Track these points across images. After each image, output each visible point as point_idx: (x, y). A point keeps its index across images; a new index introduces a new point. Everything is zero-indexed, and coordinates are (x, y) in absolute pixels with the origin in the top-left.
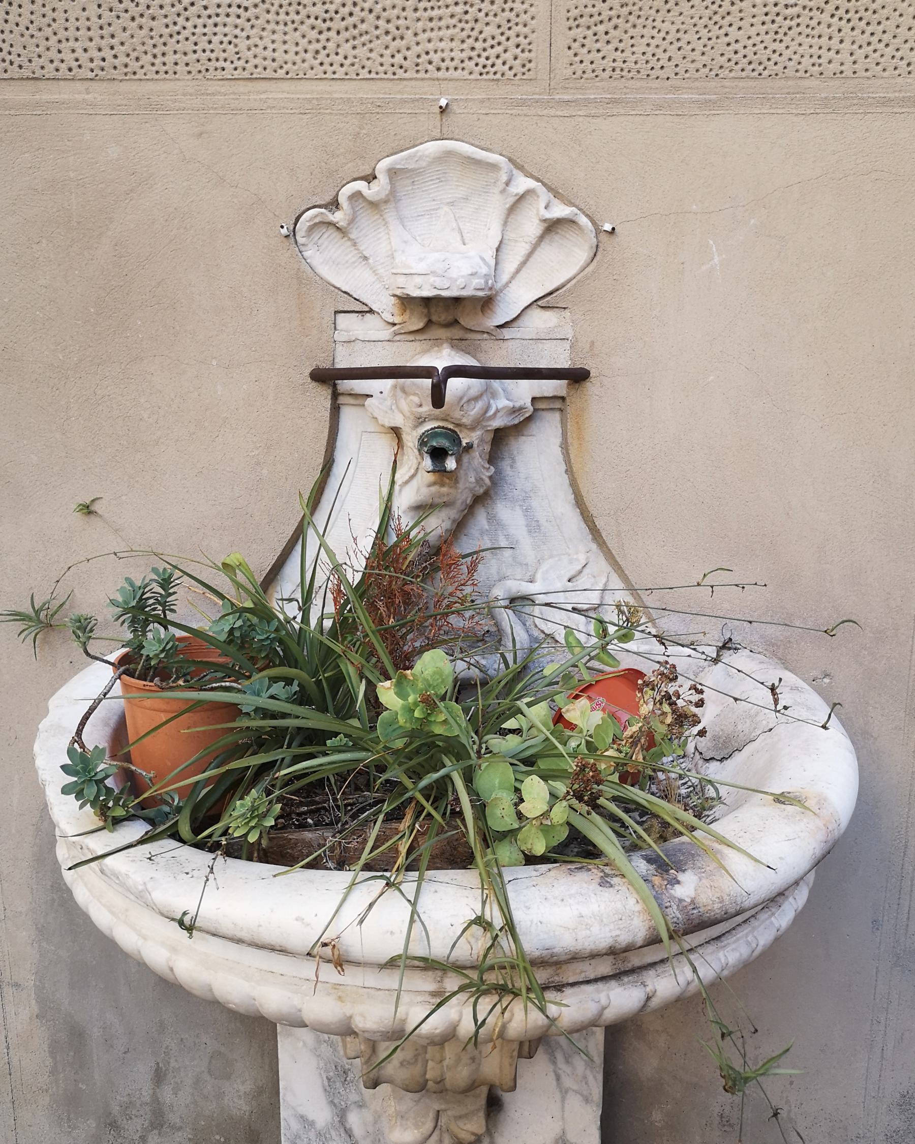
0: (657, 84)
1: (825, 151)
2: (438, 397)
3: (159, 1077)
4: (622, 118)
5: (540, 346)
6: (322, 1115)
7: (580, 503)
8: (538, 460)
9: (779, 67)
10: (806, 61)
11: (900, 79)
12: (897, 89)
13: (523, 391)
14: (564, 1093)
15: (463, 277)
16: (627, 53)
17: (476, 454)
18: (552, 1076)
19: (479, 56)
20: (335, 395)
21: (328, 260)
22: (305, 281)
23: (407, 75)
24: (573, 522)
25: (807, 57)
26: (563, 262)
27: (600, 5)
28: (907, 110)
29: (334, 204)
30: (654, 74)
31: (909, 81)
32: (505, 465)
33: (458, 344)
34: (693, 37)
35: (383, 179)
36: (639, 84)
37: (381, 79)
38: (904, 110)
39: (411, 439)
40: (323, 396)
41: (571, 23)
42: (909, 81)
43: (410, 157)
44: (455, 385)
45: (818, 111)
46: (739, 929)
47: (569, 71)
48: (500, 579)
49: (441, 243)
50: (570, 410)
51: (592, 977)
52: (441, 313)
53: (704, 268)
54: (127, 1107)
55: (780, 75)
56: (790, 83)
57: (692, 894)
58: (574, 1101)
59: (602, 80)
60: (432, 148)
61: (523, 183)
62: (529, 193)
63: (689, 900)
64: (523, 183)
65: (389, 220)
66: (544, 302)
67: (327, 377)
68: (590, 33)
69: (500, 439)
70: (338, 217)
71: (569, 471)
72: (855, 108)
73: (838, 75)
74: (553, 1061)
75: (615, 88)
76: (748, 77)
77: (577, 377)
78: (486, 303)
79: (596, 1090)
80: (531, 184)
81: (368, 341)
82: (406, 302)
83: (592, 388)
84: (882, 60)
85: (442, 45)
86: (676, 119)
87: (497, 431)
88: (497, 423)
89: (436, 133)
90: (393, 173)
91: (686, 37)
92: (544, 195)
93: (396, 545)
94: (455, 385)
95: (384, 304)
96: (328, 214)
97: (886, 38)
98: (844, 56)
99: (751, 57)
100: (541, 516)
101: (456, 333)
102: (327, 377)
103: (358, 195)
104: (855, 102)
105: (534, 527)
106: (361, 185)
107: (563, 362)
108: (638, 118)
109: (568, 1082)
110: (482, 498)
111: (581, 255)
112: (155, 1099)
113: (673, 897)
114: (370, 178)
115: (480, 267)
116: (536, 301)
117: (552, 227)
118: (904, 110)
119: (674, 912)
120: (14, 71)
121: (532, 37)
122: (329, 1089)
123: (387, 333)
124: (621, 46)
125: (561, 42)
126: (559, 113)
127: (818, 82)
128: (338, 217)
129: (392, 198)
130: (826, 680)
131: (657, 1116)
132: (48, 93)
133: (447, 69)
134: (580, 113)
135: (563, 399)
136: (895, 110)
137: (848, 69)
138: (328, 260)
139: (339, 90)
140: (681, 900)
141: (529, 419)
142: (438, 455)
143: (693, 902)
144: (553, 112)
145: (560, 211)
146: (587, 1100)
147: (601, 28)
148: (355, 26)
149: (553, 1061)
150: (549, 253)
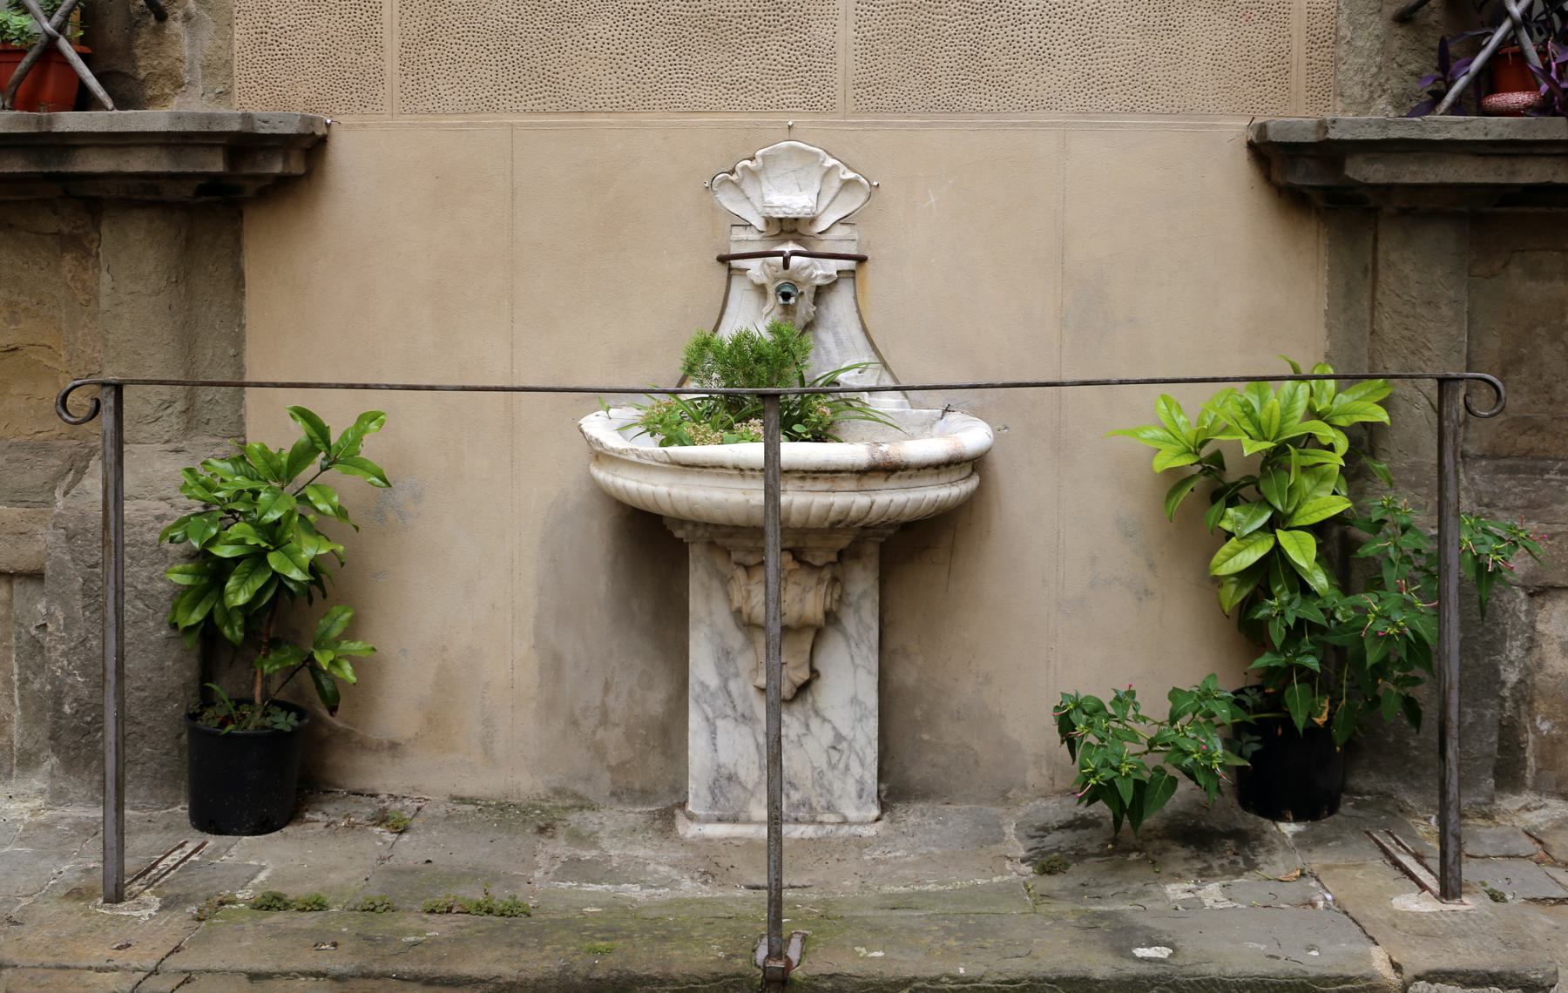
2: (786, 265)
3: (607, 688)
6: (713, 682)
7: (865, 330)
8: (841, 305)
13: (833, 266)
14: (856, 667)
17: (806, 297)
18: (848, 658)
20: (730, 269)
21: (729, 201)
22: (716, 209)
24: (861, 340)
26: (850, 203)
29: (733, 172)
32: (822, 308)
33: (797, 241)
35: (760, 160)
39: (771, 290)
40: (722, 271)
44: (795, 260)
48: (817, 369)
49: (790, 197)
50: (858, 276)
52: (789, 228)
54: (585, 709)
58: (862, 674)
60: (784, 144)
61: (830, 162)
62: (834, 167)
64: (830, 162)
66: (841, 221)
67: (724, 259)
69: (820, 293)
70: (734, 178)
71: (858, 311)
74: (849, 646)
77: (861, 260)
78: (812, 221)
79: (875, 668)
80: (835, 162)
81: (747, 240)
82: (768, 221)
83: (868, 265)
87: (818, 287)
88: (819, 282)
90: (764, 157)
92: (843, 168)
93: (619, 867)
94: (795, 260)
95: (759, 223)
96: (732, 177)
100: (843, 336)
101: (796, 236)
102: (724, 259)
103: (746, 167)
105: (839, 343)
106: (747, 163)
107: (853, 252)
109: (858, 661)
110: (809, 326)
111: (863, 198)
112: (603, 703)
114: (752, 159)
115: (574, 868)
117: (847, 184)
120: (572, 108)
122: (718, 666)
123: (757, 237)
125: (850, 95)
128: (734, 178)
129: (764, 169)
131: (918, 713)
132: (587, 119)
138: (729, 201)
139: (738, 118)
141: (836, 282)
142: (786, 296)
145: (850, 175)
146: (869, 673)
149: (849, 646)
150: (843, 197)
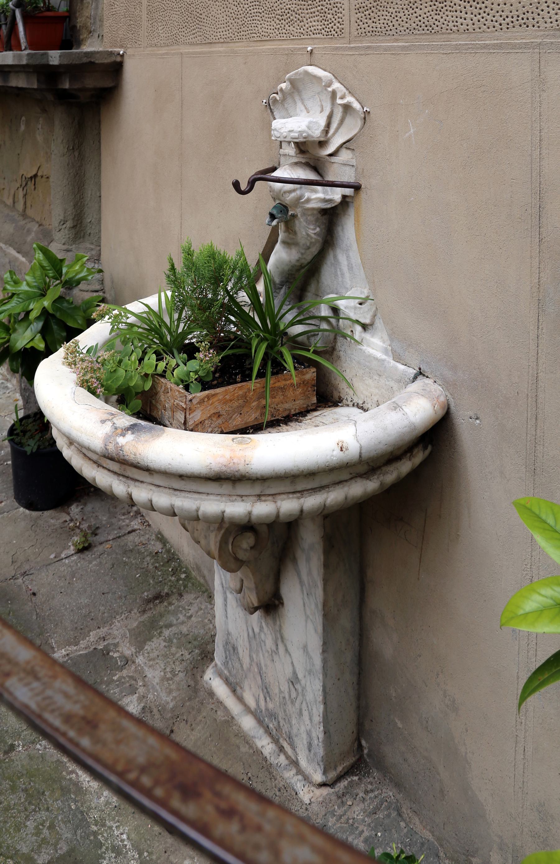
0: (388, 38)
1: (457, 73)
4: (371, 56)
5: (343, 168)
9: (439, 28)
10: (451, 24)
11: (496, 33)
12: (495, 38)
15: (285, 132)
16: (377, 24)
19: (370, 19)
23: (303, 37)
25: (451, 22)
27: (367, 2)
28: (497, 51)
30: (388, 33)
31: (501, 34)
34: (402, 14)
36: (383, 38)
37: (305, 39)
38: (495, 51)
41: (357, 11)
42: (501, 34)
43: (296, 73)
45: (453, 52)
46: (192, 494)
47: (356, 33)
51: (111, 469)
53: (407, 135)
55: (440, 32)
56: (444, 36)
57: (124, 444)
59: (368, 37)
63: (120, 445)
65: (296, 100)
68: (363, 15)
72: (470, 50)
73: (467, 31)
75: (373, 40)
76: (425, 33)
77: (357, 188)
83: (363, 194)
84: (486, 23)
85: (314, 23)
86: (393, 56)
89: (309, 63)
91: (399, 15)
97: (487, 10)
98: (468, 21)
99: (427, 23)
104: (470, 46)
108: (378, 56)
113: (115, 440)
116: (344, 143)
118: (495, 51)
119: (111, 447)
121: (343, 18)
124: (375, 20)
125: (353, 20)
126: (349, 53)
127: (457, 35)
130: (478, 421)
133: (432, 11)
134: (356, 53)
135: (353, 197)
136: (491, 51)
137: (470, 27)
140: (117, 443)
143: (122, 447)
144: (347, 53)
147: (367, 13)
148: (314, 13)
